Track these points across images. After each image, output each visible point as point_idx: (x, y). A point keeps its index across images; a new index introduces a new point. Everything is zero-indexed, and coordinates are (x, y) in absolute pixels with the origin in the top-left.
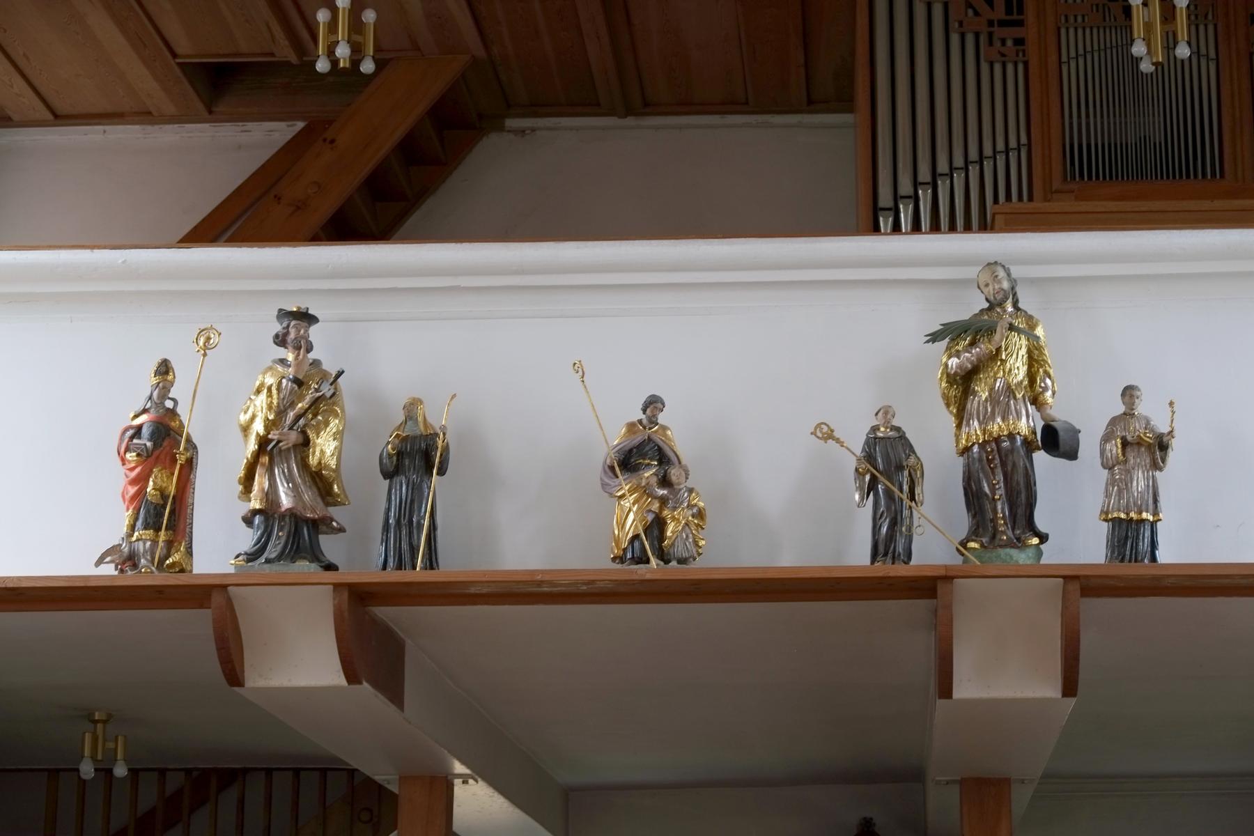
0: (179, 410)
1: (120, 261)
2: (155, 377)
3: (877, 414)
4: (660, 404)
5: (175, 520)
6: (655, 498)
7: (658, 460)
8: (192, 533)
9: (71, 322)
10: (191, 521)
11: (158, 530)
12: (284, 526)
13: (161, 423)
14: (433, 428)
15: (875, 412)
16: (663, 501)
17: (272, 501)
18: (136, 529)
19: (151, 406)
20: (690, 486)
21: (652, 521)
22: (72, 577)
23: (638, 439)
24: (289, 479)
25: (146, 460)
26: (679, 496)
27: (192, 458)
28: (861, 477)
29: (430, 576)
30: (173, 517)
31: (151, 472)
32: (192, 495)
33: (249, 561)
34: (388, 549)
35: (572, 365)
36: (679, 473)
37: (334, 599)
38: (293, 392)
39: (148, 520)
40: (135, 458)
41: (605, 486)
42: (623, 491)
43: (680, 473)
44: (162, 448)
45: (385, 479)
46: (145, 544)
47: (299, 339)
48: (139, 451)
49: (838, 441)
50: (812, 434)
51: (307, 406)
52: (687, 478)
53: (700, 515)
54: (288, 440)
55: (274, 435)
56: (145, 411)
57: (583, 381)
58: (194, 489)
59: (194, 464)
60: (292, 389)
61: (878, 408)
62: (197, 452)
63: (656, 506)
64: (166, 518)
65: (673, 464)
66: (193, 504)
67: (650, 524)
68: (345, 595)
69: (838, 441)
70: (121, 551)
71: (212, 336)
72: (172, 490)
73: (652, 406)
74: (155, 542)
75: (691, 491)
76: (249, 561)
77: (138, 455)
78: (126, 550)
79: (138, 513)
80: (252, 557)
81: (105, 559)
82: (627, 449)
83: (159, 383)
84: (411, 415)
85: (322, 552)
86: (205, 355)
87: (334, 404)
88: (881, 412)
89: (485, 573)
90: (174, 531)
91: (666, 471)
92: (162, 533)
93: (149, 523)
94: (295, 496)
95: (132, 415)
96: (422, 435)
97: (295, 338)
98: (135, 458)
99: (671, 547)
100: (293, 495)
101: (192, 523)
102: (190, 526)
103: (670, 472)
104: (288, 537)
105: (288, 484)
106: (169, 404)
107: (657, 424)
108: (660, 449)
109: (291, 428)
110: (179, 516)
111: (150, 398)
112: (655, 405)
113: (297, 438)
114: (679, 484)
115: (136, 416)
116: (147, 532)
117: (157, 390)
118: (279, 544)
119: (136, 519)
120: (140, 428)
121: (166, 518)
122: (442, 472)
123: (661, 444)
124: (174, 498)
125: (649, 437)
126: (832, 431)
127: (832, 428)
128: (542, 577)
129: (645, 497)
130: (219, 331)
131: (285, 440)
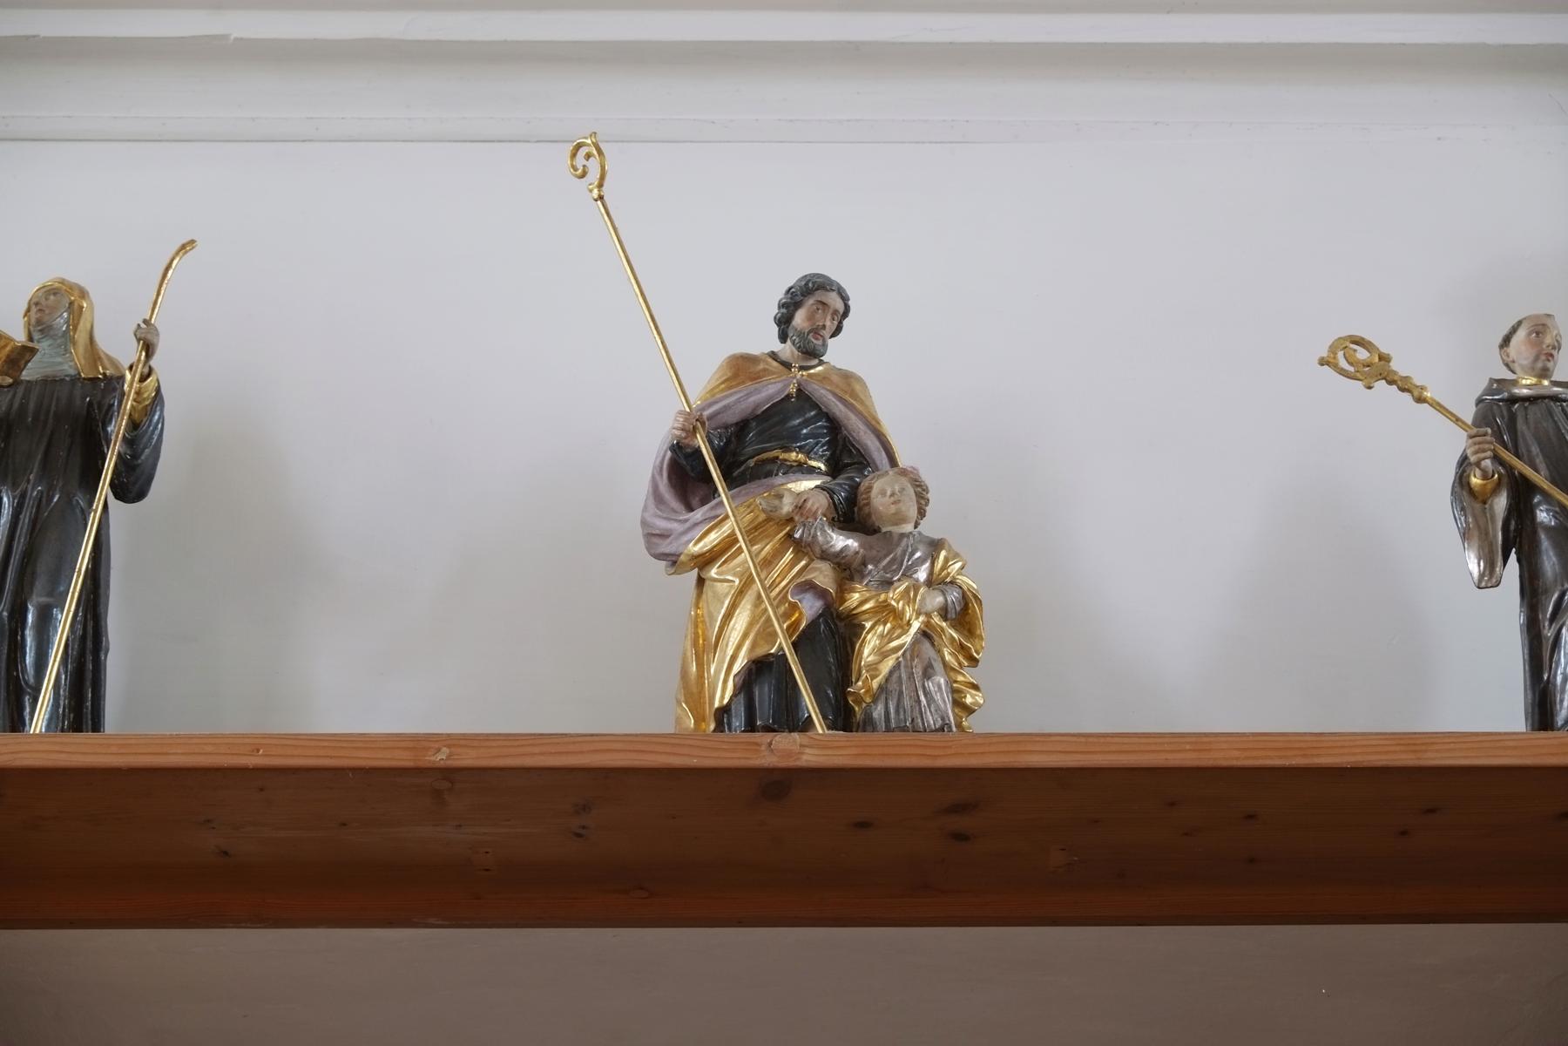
3: (1506, 341)
4: (834, 295)
6: (825, 556)
7: (828, 462)
15: (1499, 340)
16: (848, 570)
20: (936, 536)
21: (813, 624)
23: (771, 390)
26: (899, 551)
28: (1478, 506)
29: (79, 751)
35: (570, 147)
36: (897, 488)
41: (655, 540)
42: (726, 529)
43: (903, 489)
49: (1405, 386)
50: (1323, 362)
52: (922, 513)
53: (963, 615)
57: (601, 198)
61: (1514, 322)
63: (824, 576)
65: (876, 469)
67: (808, 626)
69: (1405, 386)
73: (811, 301)
75: (935, 546)
82: (732, 417)
84: (46, 319)
88: (1521, 334)
89: (256, 743)
91: (854, 489)
96: (76, 379)
99: (875, 700)
103: (870, 488)
107: (821, 363)
108: (835, 427)
112: (819, 296)
114: (900, 519)
122: (131, 486)
123: (839, 409)
125: (799, 390)
126: (1385, 358)
127: (1384, 350)
128: (449, 757)
129: (789, 556)
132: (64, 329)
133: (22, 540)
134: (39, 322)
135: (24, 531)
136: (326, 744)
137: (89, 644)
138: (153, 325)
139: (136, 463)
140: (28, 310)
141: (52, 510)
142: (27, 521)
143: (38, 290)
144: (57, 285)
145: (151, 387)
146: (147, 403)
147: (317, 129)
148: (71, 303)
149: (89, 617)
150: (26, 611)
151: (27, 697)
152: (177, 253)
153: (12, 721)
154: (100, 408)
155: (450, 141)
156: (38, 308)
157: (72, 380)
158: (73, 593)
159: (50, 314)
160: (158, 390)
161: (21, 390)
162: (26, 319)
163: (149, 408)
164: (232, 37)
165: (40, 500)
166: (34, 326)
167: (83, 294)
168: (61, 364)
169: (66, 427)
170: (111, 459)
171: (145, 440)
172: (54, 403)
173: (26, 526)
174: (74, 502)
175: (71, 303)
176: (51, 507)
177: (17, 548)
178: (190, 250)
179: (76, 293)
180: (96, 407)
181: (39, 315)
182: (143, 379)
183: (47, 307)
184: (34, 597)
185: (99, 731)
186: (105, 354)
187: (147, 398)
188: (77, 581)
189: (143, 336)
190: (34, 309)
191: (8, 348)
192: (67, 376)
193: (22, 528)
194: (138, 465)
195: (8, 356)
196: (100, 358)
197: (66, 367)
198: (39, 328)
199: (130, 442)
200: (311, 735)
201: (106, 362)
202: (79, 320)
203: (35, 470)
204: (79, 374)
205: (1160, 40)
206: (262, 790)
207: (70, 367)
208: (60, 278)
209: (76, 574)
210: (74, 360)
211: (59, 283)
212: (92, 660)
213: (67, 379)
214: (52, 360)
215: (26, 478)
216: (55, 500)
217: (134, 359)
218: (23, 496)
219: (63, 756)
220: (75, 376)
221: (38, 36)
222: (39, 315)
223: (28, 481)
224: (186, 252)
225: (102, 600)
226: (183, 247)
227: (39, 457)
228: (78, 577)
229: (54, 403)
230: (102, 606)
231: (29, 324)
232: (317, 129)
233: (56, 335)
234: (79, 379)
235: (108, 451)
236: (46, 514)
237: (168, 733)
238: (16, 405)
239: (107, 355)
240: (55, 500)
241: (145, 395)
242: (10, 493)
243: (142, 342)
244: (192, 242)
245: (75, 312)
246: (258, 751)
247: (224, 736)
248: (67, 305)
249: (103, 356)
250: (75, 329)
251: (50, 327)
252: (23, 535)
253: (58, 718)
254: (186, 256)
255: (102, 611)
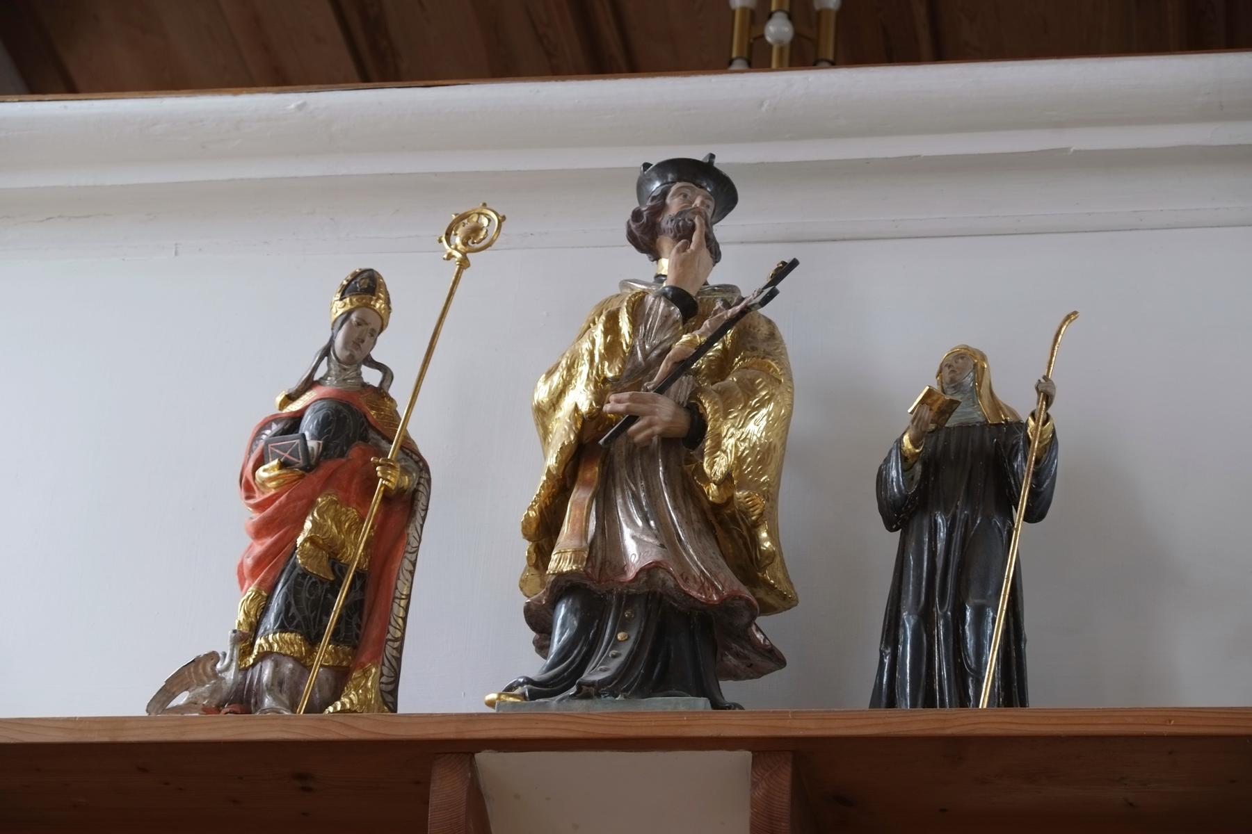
0: (393, 392)
1: (293, 106)
2: (341, 299)
5: (359, 627)
8: (399, 660)
9: (176, 254)
10: (399, 634)
11: (312, 640)
12: (630, 619)
13: (348, 406)
14: (1013, 413)
17: (603, 564)
18: (261, 631)
19: (327, 375)
22: (82, 720)
24: (652, 511)
25: (302, 477)
27: (416, 491)
29: (1010, 722)
30: (356, 617)
31: (311, 504)
32: (408, 576)
33: (533, 696)
34: (897, 683)
37: (754, 785)
38: (670, 322)
39: (293, 610)
40: (277, 472)
44: (343, 460)
45: (890, 525)
46: (277, 665)
47: (689, 215)
48: (286, 455)
51: (703, 339)
54: (653, 413)
55: (618, 401)
56: (309, 384)
58: (414, 564)
59: (420, 506)
60: (667, 316)
62: (429, 481)
64: (333, 617)
66: (408, 597)
68: (785, 778)
70: (215, 675)
71: (485, 221)
72: (356, 553)
74: (304, 666)
76: (533, 696)
77: (284, 465)
78: (230, 676)
79: (269, 598)
80: (540, 689)
81: (174, 696)
83: (349, 313)
84: (958, 378)
85: (721, 693)
86: (464, 264)
87: (768, 354)
90: (355, 647)
92: (325, 645)
93: (293, 617)
94: (662, 546)
95: (279, 399)
96: (985, 425)
97: (680, 214)
98: (277, 472)
100: (657, 543)
101: (402, 639)
102: (397, 644)
104: (640, 643)
105: (646, 520)
106: (372, 377)
109: (661, 389)
110: (370, 614)
111: (326, 352)
113: (675, 415)
115: (291, 398)
116: (287, 636)
117: (344, 326)
118: (614, 657)
119: (264, 610)
120: (296, 419)
121: (333, 617)
122: (1035, 514)
124: (359, 575)
130: (501, 214)
131: (644, 414)
132: (971, 385)
133: (957, 554)
134: (952, 380)
135: (958, 546)
136: (1225, 716)
137: (1012, 637)
138: (1050, 380)
139: (1039, 490)
140: (940, 371)
141: (976, 530)
142: (958, 539)
143: (948, 355)
144: (963, 351)
145: (1049, 431)
146: (1046, 443)
147: (1141, 220)
148: (975, 365)
149: (1010, 614)
150: (965, 609)
151: (970, 679)
152: (1064, 322)
153: (960, 698)
154: (1005, 447)
155: (1148, 229)
156: (951, 369)
157: (981, 426)
158: (1004, 595)
159: (961, 373)
160: (1054, 432)
161: (942, 435)
162: (938, 378)
163: (1048, 447)
164: (1072, 150)
165: (967, 521)
166: (947, 384)
167: (984, 358)
168: (971, 413)
169: (981, 463)
170: (1025, 488)
171: (1046, 472)
172: (970, 444)
173: (958, 543)
174: (993, 523)
175: (975, 365)
176: (975, 527)
177: (953, 561)
178: (1074, 319)
179: (978, 357)
180: (1002, 447)
181: (952, 375)
182: (1044, 424)
183: (958, 368)
184: (970, 599)
185: (1025, 706)
186: (1004, 404)
187: (1046, 439)
188: (1006, 587)
189: (1044, 389)
190: (947, 371)
191: (940, 402)
192: (977, 423)
193: (955, 544)
194: (1042, 492)
195: (939, 408)
196: (1001, 408)
197: (975, 416)
198: (953, 385)
199: (1037, 475)
200: (1190, 708)
201: (1006, 411)
202: (982, 377)
203: (961, 498)
204: (986, 421)
205: (944, 153)
206: (1171, 753)
207: (979, 415)
208: (966, 345)
209: (1005, 580)
210: (981, 409)
211: (965, 349)
212: (1015, 649)
213: (978, 425)
214: (965, 410)
215: (954, 505)
216: (978, 522)
217: (1033, 406)
218: (954, 518)
219: (1014, 727)
220: (983, 422)
221: (919, 156)
222: (952, 375)
223: (957, 507)
224: (1071, 321)
225: (1019, 600)
226: (1068, 317)
227: (964, 487)
228: (1007, 582)
229: (970, 444)
230: (1019, 606)
231: (942, 382)
232: (1141, 220)
233: (965, 391)
234: (986, 425)
235: (1023, 479)
236: (972, 533)
237: (1096, 707)
238: (940, 447)
239: (1006, 406)
240: (978, 522)
241: (1045, 437)
242: (943, 517)
243: (1042, 394)
244: (1075, 313)
245: (979, 372)
246: (1170, 721)
247: (1141, 710)
248: (972, 367)
249: (1003, 406)
250: (980, 386)
251: (961, 384)
252: (957, 551)
253: (995, 696)
254: (325, 342)
255: (1020, 609)
